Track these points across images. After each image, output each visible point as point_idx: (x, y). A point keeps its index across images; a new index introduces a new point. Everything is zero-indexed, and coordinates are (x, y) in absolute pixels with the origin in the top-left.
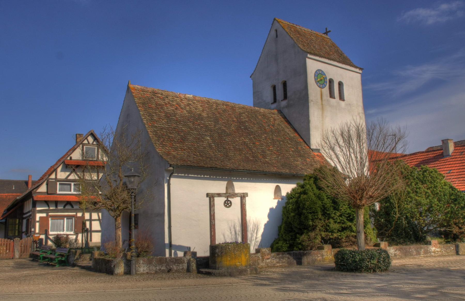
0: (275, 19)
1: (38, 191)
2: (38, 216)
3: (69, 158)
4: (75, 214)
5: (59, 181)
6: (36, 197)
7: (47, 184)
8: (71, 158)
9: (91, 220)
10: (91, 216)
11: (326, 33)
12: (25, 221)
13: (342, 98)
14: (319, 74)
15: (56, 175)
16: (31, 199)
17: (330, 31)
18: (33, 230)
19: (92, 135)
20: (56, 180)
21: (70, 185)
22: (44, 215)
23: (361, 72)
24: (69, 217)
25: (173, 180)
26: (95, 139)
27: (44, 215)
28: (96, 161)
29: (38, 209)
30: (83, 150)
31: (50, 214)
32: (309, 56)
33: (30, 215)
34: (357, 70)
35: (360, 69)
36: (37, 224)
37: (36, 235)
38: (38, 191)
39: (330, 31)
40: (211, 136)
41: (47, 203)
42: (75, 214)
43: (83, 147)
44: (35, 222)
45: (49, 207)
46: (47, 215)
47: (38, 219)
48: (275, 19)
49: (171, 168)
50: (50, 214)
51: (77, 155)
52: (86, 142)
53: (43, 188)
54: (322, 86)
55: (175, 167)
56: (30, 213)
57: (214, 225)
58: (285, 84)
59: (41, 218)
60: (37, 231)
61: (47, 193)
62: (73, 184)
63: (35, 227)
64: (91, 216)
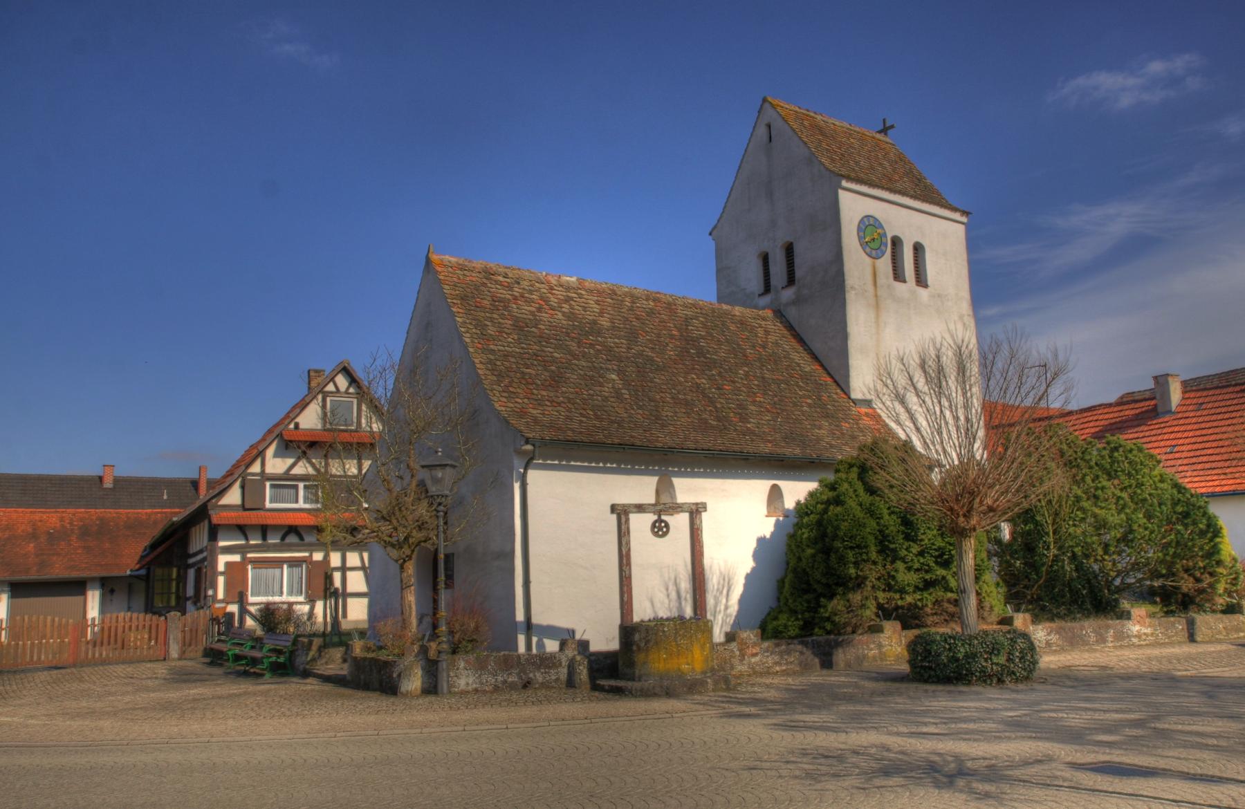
0: (765, 100)
2: (222, 560)
3: (292, 426)
4: (307, 554)
5: (269, 479)
7: (243, 487)
8: (297, 426)
9: (344, 569)
11: (884, 131)
12: (191, 573)
13: (921, 280)
16: (206, 522)
17: (892, 127)
18: (210, 592)
19: (346, 371)
20: (264, 476)
21: (296, 487)
22: (236, 558)
23: (964, 219)
24: (294, 563)
26: (353, 380)
27: (236, 558)
28: (356, 431)
29: (222, 544)
31: (249, 555)
33: (205, 559)
34: (957, 216)
35: (964, 213)
36: (221, 580)
37: (218, 605)
39: (892, 127)
40: (621, 372)
41: (242, 530)
42: (307, 554)
43: (324, 400)
44: (215, 574)
45: (247, 539)
46: (244, 558)
47: (221, 567)
48: (765, 100)
49: (529, 447)
50: (249, 555)
51: (310, 419)
52: (330, 387)
53: (233, 497)
54: (875, 254)
56: (205, 554)
59: (228, 564)
60: (221, 595)
61: (243, 507)
62: (301, 485)
63: (215, 588)
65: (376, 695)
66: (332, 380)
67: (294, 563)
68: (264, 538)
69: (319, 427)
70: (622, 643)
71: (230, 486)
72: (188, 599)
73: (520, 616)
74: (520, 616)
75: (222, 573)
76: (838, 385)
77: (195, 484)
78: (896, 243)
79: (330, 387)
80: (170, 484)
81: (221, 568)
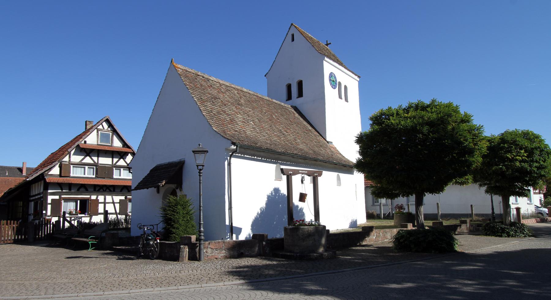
0: (292, 24)
1: (50, 173)
2: (50, 198)
3: (83, 142)
4: (89, 196)
5: (72, 164)
6: (48, 179)
7: (60, 167)
8: (85, 142)
9: (105, 203)
10: (105, 199)
11: (327, 45)
12: (32, 204)
13: (346, 100)
14: (331, 75)
15: (70, 157)
16: (43, 182)
17: (330, 44)
18: (44, 212)
19: (108, 121)
20: (70, 163)
21: (85, 168)
22: (57, 197)
23: (358, 79)
24: (75, 200)
25: (233, 160)
26: (110, 125)
27: (57, 197)
28: (111, 146)
29: (49, 191)
30: (98, 135)
31: (62, 196)
32: (326, 59)
33: (42, 197)
34: (356, 77)
35: (359, 77)
36: (49, 207)
37: (47, 218)
38: (50, 173)
39: (330, 44)
40: (253, 121)
41: (60, 186)
42: (89, 196)
43: (98, 132)
44: (47, 204)
45: (62, 190)
46: (60, 197)
47: (49, 201)
48: (292, 24)
49: (233, 147)
50: (62, 196)
51: (92, 140)
52: (100, 127)
53: (56, 171)
54: (334, 87)
55: (239, 146)
56: (42, 195)
57: (318, 209)
58: (300, 84)
59: (52, 200)
60: (49, 213)
61: (60, 175)
62: (87, 167)
63: (46, 210)
64: (105, 199)
65: (156, 261)
66: (102, 124)
67: (75, 200)
68: (70, 189)
69: (96, 143)
70: (463, 254)
71: (54, 166)
72: (30, 215)
73: (227, 223)
74: (227, 223)
75: (49, 204)
76: (321, 135)
77: (20, 170)
78: (340, 83)
79: (100, 127)
80: (10, 169)
81: (49, 201)
